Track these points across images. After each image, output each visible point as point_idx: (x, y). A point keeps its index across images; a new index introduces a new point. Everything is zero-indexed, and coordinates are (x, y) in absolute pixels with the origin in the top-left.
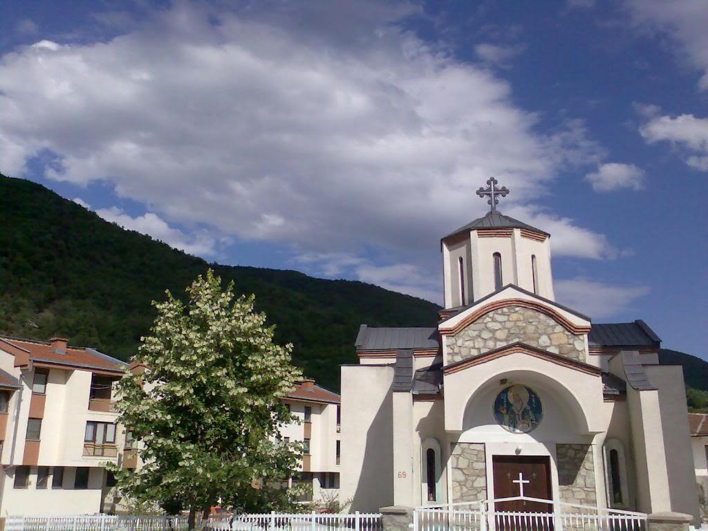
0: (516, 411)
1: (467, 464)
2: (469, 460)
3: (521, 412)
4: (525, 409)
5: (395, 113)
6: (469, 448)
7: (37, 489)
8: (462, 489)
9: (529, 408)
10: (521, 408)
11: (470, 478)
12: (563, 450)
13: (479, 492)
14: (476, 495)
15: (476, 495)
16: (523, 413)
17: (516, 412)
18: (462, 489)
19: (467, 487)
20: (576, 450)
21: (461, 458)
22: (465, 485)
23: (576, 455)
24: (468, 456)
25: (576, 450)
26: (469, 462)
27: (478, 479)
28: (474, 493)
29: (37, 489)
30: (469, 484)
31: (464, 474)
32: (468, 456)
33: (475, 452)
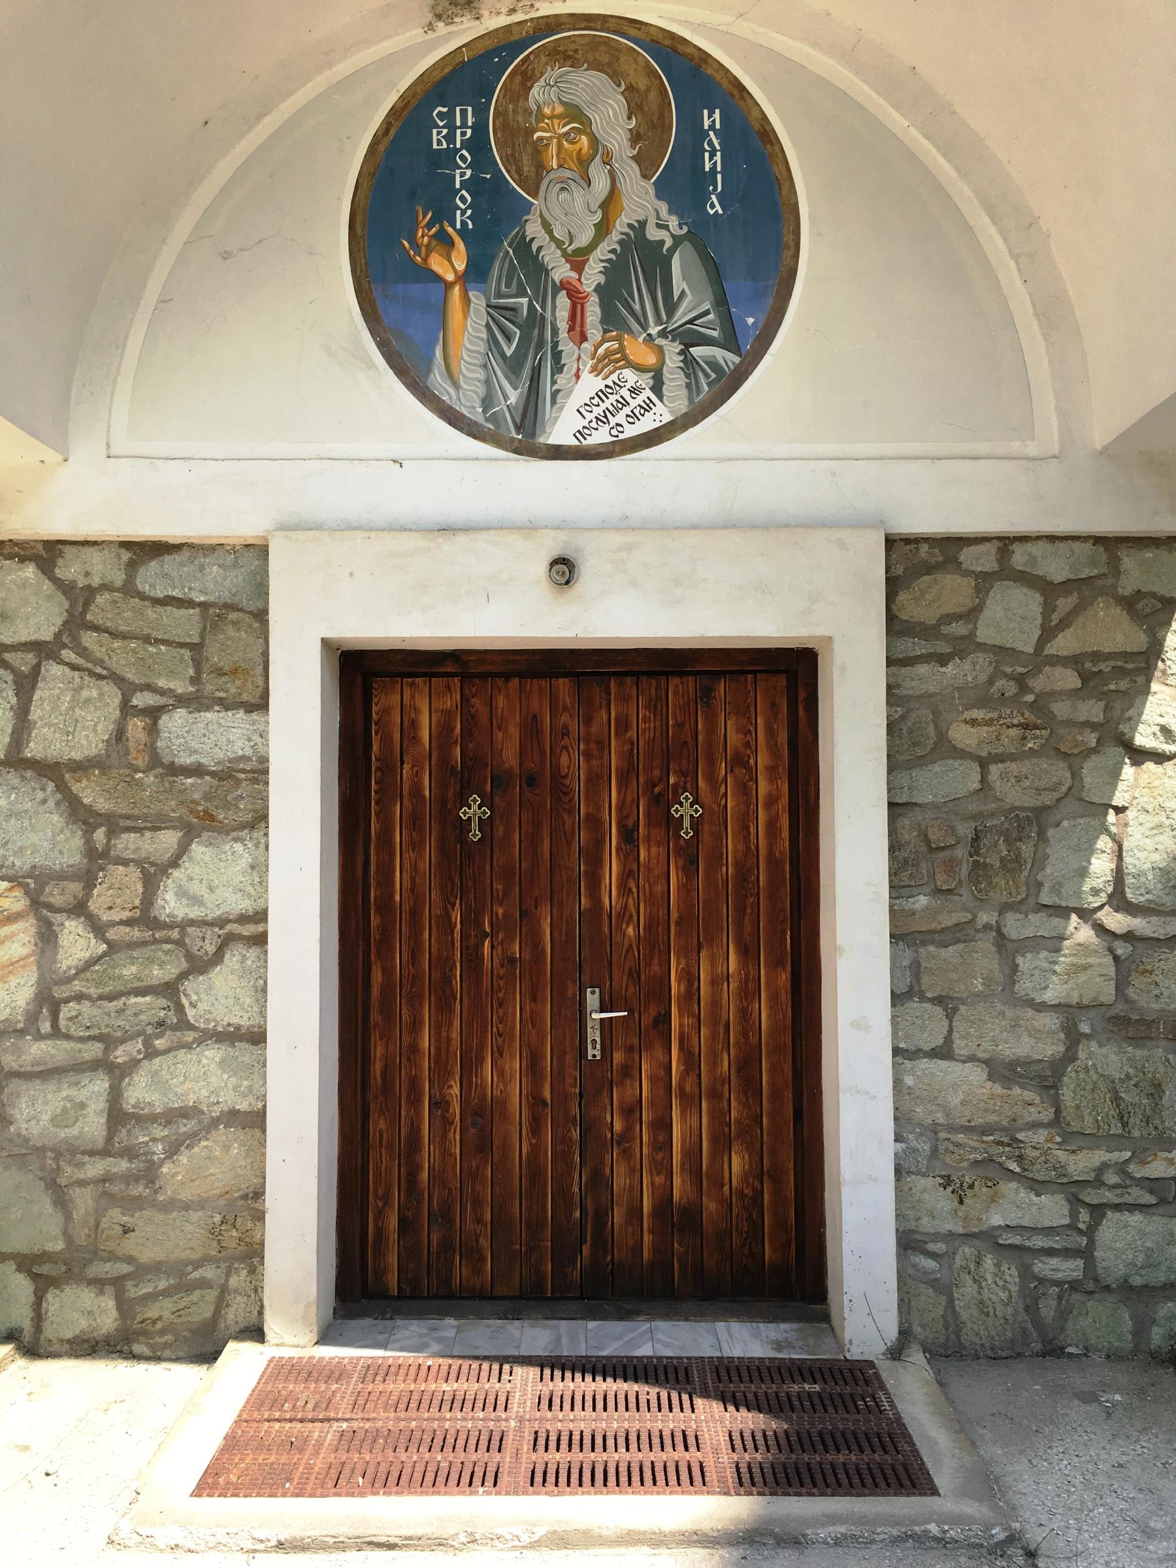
0: (552, 257)
1: (105, 729)
2: (127, 689)
3: (593, 276)
4: (637, 236)
5: (98, 1113)
6: (129, 590)
7: (326, 643)
8: (47, 937)
9: (665, 226)
10: (603, 229)
11: (127, 844)
12: (946, 593)
13: (199, 966)
14: (170, 990)
15: (170, 990)
16: (616, 273)
17: (561, 271)
18: (47, 937)
19: (98, 929)
20: (1048, 589)
21: (53, 670)
22: (79, 909)
23: (1048, 633)
24: (121, 657)
25: (1048, 589)
26: (126, 708)
27: (198, 850)
28: (158, 974)
29: (326, 643)
30: (115, 894)
31: (80, 815)
32: (121, 657)
33: (186, 624)
